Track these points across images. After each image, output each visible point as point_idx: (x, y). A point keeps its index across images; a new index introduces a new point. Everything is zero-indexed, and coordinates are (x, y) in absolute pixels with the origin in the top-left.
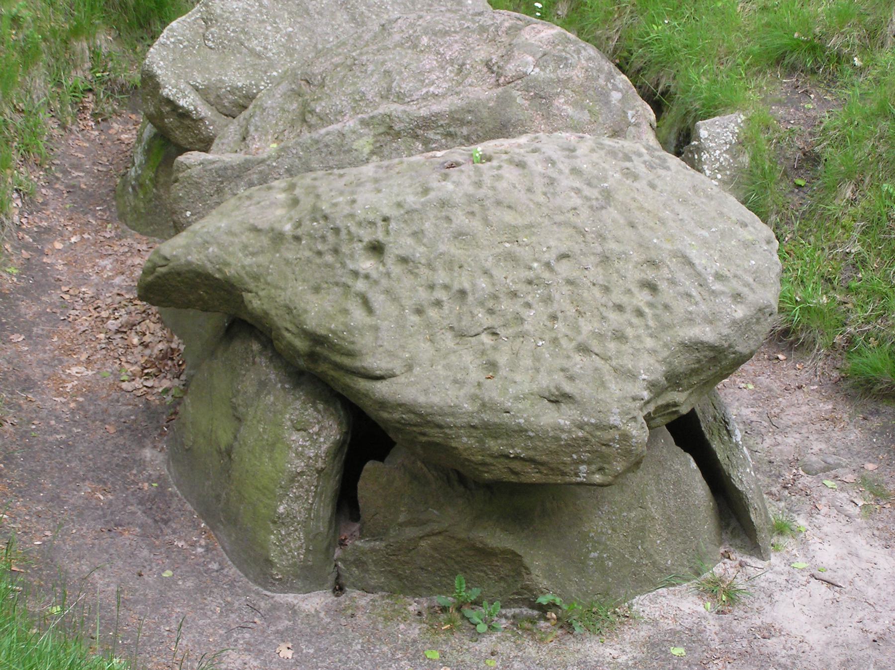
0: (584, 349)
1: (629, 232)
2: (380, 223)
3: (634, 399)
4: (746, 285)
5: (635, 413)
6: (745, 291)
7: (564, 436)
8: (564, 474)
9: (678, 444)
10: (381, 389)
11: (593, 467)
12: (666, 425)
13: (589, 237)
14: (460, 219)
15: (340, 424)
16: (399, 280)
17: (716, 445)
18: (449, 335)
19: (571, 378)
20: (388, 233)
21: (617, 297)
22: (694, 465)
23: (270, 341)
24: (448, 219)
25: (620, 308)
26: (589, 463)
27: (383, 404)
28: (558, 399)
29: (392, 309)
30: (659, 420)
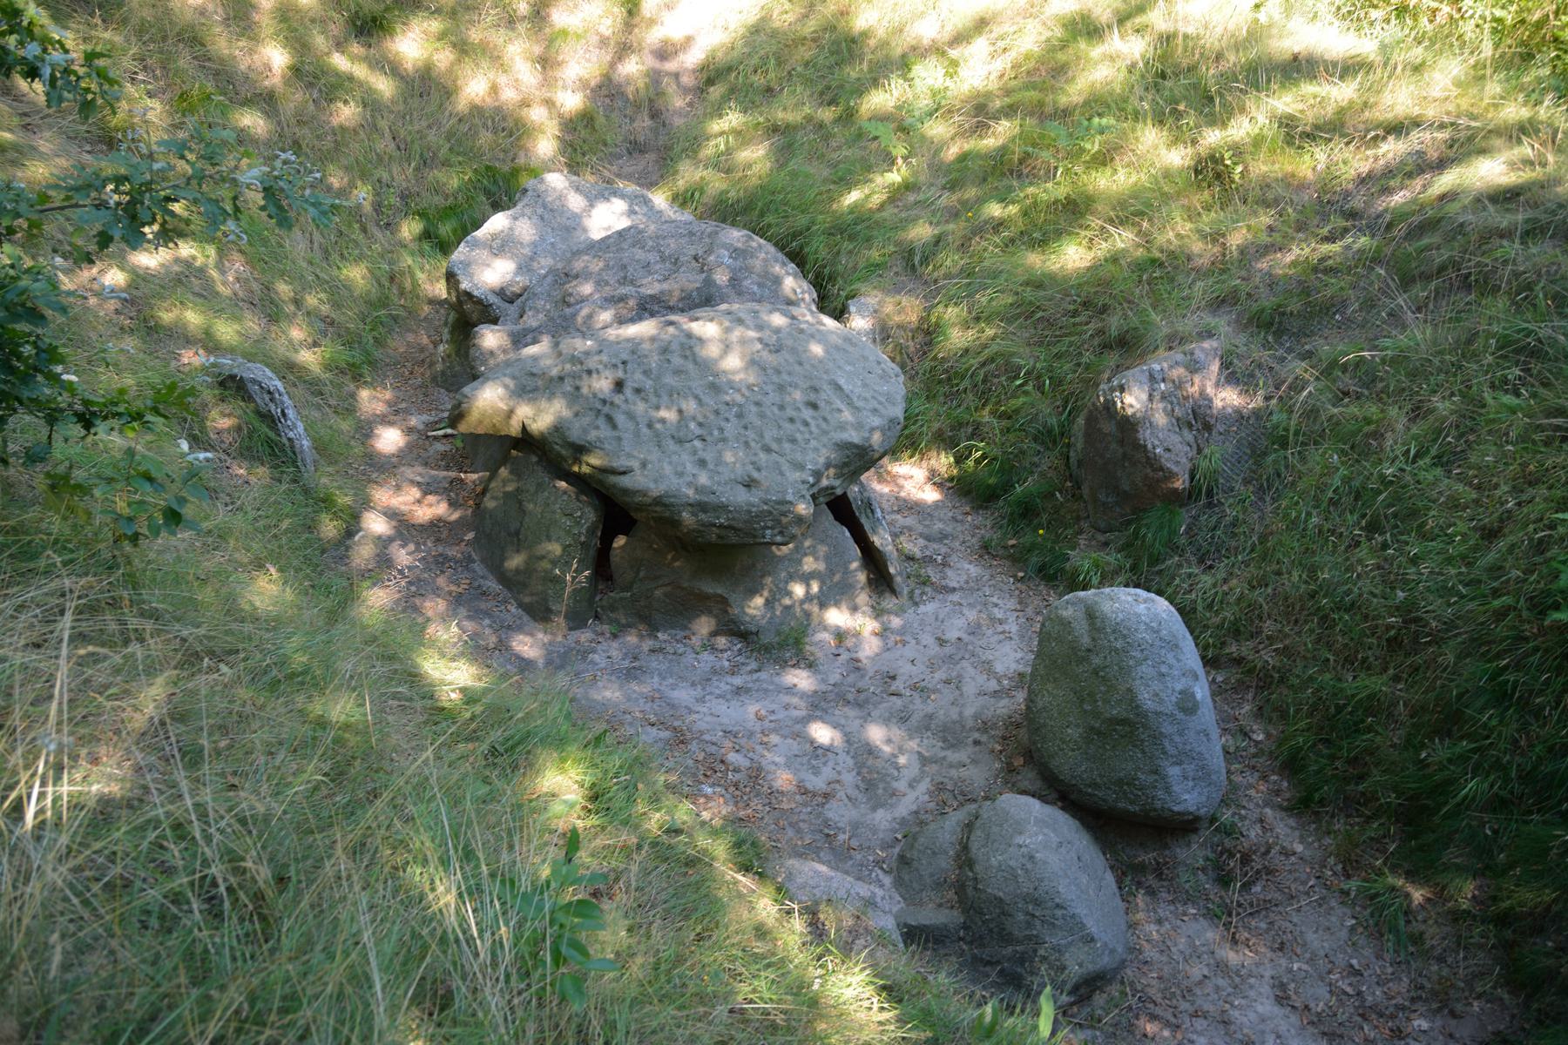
0: (768, 450)
1: (797, 368)
2: (620, 365)
3: (803, 482)
4: (880, 403)
5: (804, 492)
6: (879, 407)
7: (754, 509)
8: (755, 537)
9: (836, 519)
10: (625, 481)
11: (776, 531)
12: (827, 504)
13: (769, 371)
14: (677, 360)
15: (596, 510)
16: (635, 404)
17: (863, 520)
18: (671, 442)
19: (759, 470)
20: (625, 372)
21: (790, 412)
22: (848, 534)
23: (544, 453)
24: (669, 361)
25: (792, 420)
26: (772, 528)
27: (626, 491)
28: (749, 484)
29: (631, 425)
30: (821, 499)
